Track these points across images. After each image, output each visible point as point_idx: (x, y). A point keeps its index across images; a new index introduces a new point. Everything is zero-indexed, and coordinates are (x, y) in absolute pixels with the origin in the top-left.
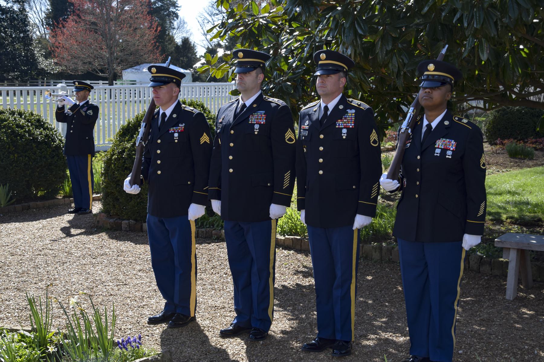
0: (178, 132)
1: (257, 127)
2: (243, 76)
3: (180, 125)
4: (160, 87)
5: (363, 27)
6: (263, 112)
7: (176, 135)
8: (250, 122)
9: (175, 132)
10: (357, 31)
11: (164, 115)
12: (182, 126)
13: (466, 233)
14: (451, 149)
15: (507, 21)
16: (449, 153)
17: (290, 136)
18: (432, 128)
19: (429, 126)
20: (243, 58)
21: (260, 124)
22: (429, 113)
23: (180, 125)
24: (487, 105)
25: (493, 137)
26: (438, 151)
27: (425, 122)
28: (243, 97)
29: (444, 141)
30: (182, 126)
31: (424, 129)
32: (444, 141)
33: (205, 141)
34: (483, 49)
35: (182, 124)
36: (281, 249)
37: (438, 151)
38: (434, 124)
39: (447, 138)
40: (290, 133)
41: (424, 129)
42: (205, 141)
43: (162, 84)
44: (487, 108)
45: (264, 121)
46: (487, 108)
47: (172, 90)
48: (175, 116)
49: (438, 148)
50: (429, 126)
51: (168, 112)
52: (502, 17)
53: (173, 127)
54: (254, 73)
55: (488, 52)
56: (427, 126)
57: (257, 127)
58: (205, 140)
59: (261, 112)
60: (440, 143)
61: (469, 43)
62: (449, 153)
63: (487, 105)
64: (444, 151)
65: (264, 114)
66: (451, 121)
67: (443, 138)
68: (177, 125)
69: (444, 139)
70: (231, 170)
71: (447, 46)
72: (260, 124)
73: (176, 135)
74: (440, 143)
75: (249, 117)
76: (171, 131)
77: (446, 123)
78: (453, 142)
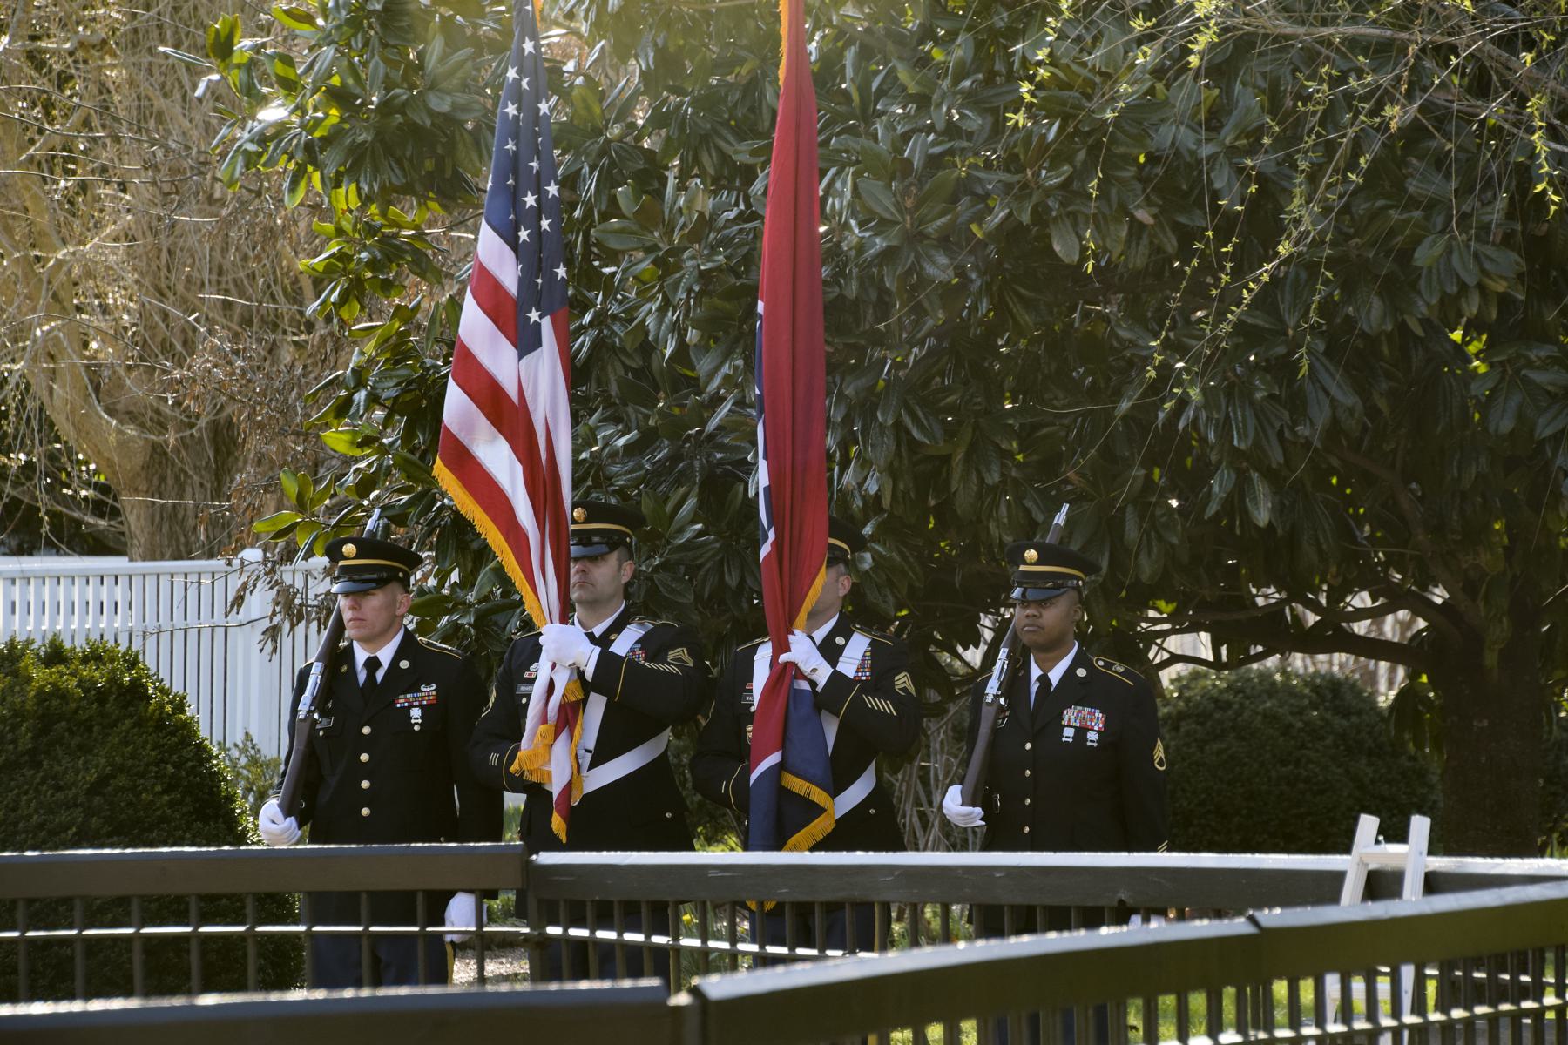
0: (420, 706)
2: (588, 564)
3: (423, 688)
4: (366, 593)
5: (925, 423)
7: (416, 713)
9: (412, 706)
10: (909, 433)
11: (373, 664)
12: (429, 690)
14: (1096, 728)
15: (1307, 433)
16: (1092, 736)
18: (1050, 684)
19: (1044, 680)
20: (585, 522)
22: (1043, 656)
23: (423, 688)
24: (1224, 650)
25: (1181, 704)
26: (1069, 733)
27: (1036, 672)
28: (583, 620)
29: (1080, 712)
30: (429, 690)
31: (1034, 687)
32: (1080, 712)
34: (1255, 498)
35: (428, 684)
37: (1069, 733)
38: (1055, 676)
39: (1084, 706)
41: (1034, 687)
43: (374, 585)
44: (1224, 658)
46: (1224, 658)
47: (394, 600)
48: (404, 664)
49: (1068, 726)
50: (1044, 680)
51: (386, 654)
52: (1295, 423)
53: (405, 693)
54: (613, 558)
55: (1270, 505)
56: (1039, 679)
60: (1072, 716)
61: (1221, 481)
62: (1092, 736)
63: (1224, 650)
64: (1081, 732)
66: (1090, 667)
67: (1077, 704)
69: (1079, 708)
71: (1066, 507)
73: (416, 713)
74: (1072, 716)
76: (401, 702)
77: (1081, 672)
78: (1098, 714)
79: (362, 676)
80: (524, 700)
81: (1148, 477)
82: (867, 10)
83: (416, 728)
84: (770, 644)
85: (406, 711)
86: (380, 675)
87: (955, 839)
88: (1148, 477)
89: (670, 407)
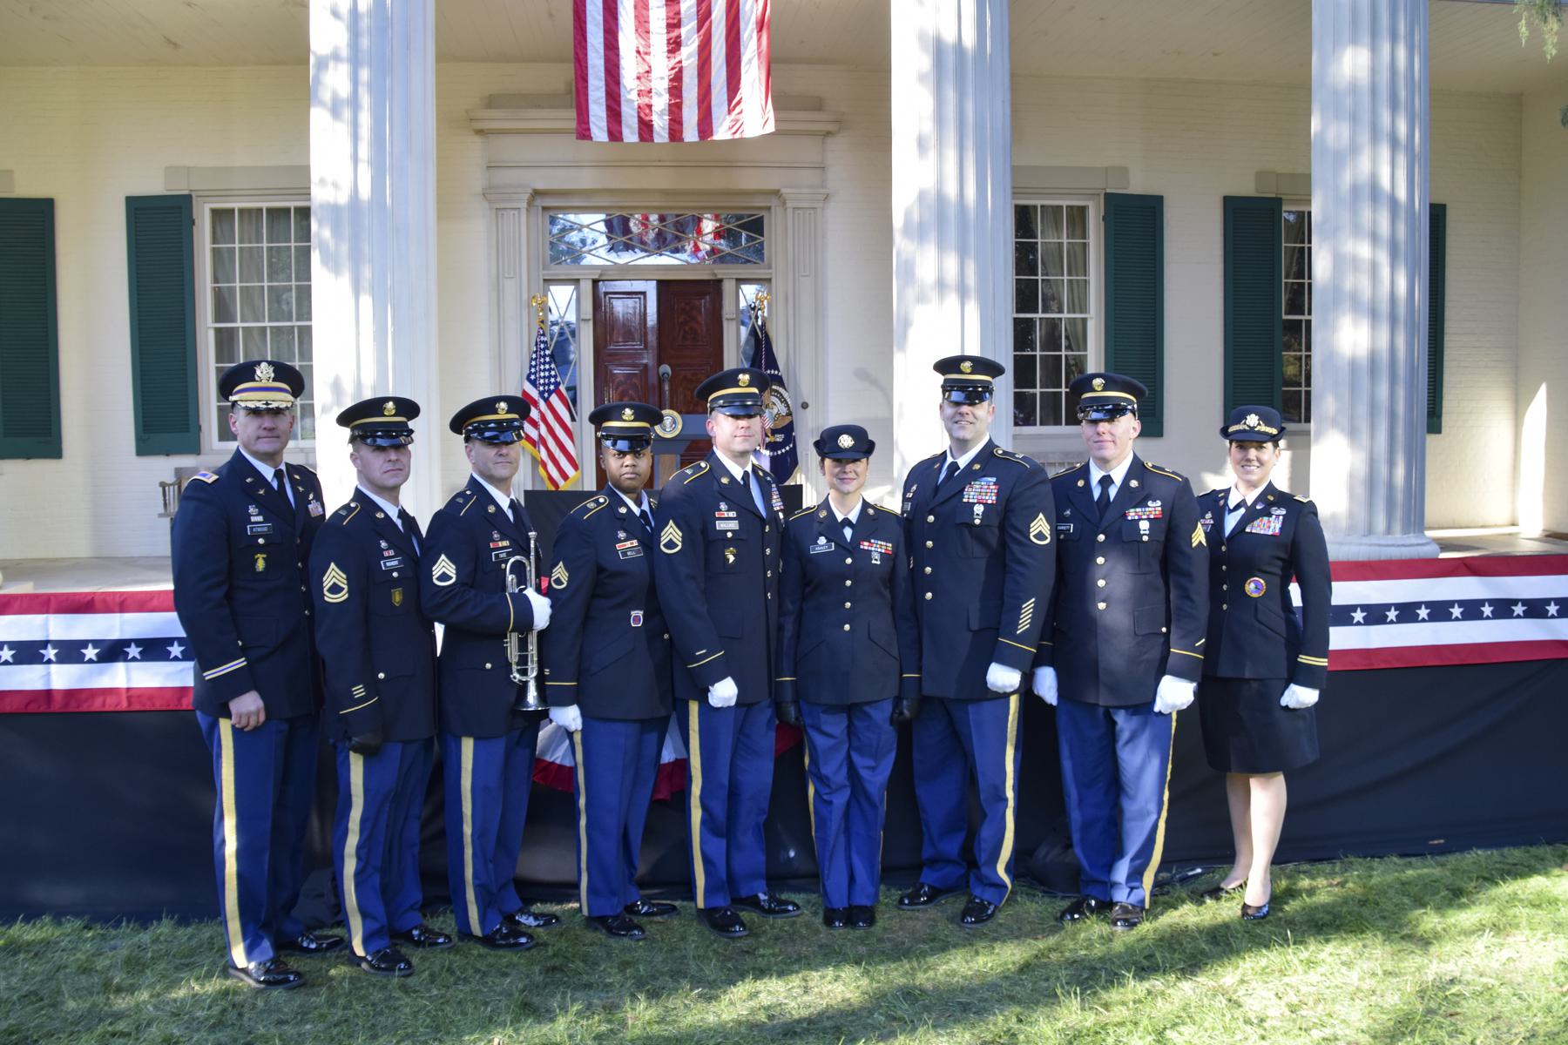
0: (1148, 519)
1: (979, 509)
3: (1150, 503)
6: (994, 479)
8: (965, 500)
9: (1140, 519)
11: (1106, 481)
12: (1155, 507)
13: (1055, 669)
17: (1040, 528)
21: (985, 505)
30: (1155, 507)
33: (335, 583)
35: (1154, 501)
36: (155, 922)
40: (671, 530)
42: (335, 583)
45: (994, 498)
53: (1135, 507)
57: (979, 509)
58: (334, 580)
59: (990, 479)
65: (995, 484)
67: (1524, 845)
68: (1142, 503)
70: (488, 666)
72: (985, 505)
73: (1144, 526)
75: (963, 490)
79: (1097, 493)
80: (871, 511)
81: (500, 929)
82: (977, 901)
83: (977, 522)
84: (898, 511)
85: (1136, 522)
86: (1113, 492)
87: (692, 475)
88: (500, 929)
89: (730, 542)
